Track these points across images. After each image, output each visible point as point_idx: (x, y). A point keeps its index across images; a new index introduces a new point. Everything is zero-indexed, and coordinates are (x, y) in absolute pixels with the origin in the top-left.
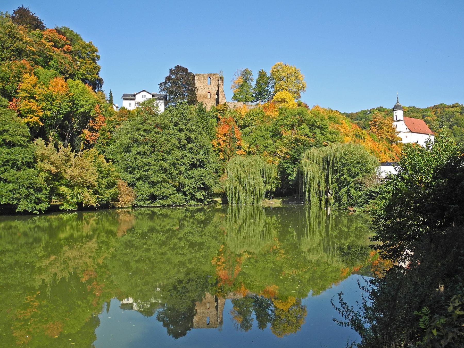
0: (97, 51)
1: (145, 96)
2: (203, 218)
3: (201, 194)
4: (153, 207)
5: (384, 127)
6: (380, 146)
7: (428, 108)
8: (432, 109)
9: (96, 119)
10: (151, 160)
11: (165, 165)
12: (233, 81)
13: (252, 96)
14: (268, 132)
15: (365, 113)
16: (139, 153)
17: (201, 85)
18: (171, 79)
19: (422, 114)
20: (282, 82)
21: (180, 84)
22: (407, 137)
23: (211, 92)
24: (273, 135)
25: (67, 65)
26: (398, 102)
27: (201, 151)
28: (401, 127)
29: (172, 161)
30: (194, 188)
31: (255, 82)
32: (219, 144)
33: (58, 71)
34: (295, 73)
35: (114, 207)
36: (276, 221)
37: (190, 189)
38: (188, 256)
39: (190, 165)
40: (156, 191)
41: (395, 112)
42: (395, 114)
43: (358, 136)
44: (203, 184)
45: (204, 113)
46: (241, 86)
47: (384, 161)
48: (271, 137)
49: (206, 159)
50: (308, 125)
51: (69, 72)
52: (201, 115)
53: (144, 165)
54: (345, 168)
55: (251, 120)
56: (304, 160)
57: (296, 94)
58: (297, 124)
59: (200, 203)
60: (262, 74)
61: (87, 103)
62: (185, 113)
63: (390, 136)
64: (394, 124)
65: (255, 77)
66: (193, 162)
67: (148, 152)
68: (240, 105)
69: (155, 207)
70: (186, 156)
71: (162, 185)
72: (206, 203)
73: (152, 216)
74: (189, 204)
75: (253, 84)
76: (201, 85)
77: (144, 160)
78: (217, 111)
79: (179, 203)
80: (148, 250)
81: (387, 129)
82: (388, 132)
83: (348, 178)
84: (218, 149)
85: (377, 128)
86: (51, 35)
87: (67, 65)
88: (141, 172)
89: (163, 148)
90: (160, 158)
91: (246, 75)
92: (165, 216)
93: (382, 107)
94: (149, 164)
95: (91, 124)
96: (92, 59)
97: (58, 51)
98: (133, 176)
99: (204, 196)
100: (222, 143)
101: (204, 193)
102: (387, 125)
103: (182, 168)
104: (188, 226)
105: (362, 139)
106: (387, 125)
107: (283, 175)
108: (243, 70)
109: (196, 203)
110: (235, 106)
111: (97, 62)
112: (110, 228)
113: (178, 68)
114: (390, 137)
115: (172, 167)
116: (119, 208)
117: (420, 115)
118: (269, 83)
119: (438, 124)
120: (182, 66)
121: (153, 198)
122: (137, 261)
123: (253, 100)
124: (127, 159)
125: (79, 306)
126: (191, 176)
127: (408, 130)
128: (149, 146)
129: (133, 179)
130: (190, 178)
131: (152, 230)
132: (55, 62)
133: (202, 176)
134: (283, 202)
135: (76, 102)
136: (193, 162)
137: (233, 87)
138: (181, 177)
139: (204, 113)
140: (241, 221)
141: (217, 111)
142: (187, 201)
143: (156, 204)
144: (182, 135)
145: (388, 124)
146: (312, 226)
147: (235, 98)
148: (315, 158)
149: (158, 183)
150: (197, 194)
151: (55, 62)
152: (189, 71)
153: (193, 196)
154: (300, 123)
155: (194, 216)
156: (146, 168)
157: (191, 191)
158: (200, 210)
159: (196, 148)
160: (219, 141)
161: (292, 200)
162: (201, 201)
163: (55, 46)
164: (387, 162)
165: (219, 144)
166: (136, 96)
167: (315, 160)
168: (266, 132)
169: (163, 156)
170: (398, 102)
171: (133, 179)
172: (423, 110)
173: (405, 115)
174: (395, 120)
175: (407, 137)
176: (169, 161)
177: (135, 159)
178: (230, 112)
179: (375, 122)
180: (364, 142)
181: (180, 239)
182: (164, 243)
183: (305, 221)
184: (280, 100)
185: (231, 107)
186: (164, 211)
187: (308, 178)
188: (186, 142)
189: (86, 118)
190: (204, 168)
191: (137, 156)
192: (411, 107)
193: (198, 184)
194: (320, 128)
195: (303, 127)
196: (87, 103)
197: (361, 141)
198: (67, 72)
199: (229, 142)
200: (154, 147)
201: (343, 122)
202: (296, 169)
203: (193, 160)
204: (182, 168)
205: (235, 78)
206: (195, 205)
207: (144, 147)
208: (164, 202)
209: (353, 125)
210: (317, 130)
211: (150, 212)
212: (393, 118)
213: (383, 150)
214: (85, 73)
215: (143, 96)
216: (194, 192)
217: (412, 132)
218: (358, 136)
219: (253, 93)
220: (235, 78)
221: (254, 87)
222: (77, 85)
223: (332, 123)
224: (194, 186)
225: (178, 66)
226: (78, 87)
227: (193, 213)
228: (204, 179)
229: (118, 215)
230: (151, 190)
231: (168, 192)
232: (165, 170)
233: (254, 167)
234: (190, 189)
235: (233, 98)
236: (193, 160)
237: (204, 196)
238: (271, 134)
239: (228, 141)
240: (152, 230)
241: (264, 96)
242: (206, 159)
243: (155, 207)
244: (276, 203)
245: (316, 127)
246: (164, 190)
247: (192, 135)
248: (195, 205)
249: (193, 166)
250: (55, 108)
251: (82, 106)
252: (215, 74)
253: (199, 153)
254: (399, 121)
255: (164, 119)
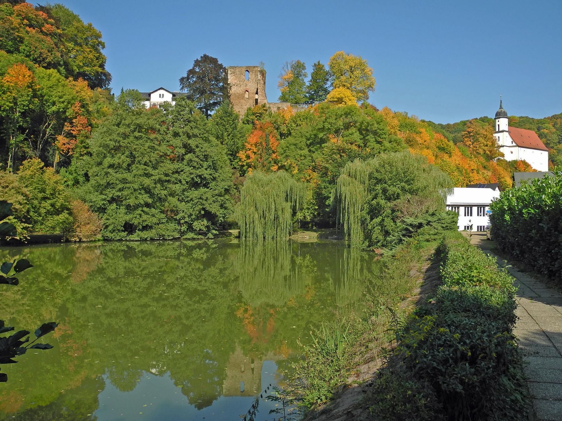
0: (100, 37)
1: (163, 95)
2: (205, 257)
3: (202, 223)
4: (130, 241)
5: (480, 139)
6: (472, 163)
7: (545, 118)
8: (551, 120)
9: (74, 121)
10: (128, 176)
11: (147, 182)
12: (281, 76)
13: (306, 96)
14: (304, 140)
15: (464, 123)
16: (111, 166)
17: (236, 81)
18: (196, 72)
19: (538, 126)
20: (343, 78)
21: (207, 81)
22: (512, 153)
23: (249, 91)
24: (311, 144)
25: (45, 51)
26: (501, 108)
27: (205, 164)
28: (504, 139)
29: (157, 178)
30: (191, 215)
31: (310, 78)
32: (248, 157)
33: (31, 57)
34: (361, 66)
35: (68, 241)
36: (311, 262)
37: (186, 216)
38: (185, 310)
39: (187, 183)
40: (135, 218)
41: (497, 120)
42: (497, 123)
43: (442, 149)
44: (204, 209)
45: (229, 116)
46: (291, 84)
47: (476, 182)
48: (308, 146)
49: (210, 175)
50: (360, 130)
51: (47, 60)
52: (225, 119)
53: (118, 182)
54: (379, 187)
55: (297, 126)
56: (343, 177)
57: (363, 94)
58: (343, 127)
59: (200, 236)
60: (318, 67)
61: (61, 100)
62: (182, 111)
63: (489, 151)
64: (496, 135)
65: (309, 70)
66: (193, 179)
67: (125, 165)
68: (286, 106)
69: (133, 241)
70: (182, 171)
71: (142, 211)
72: (210, 235)
73: (129, 253)
74: (185, 237)
75: (307, 80)
76: (236, 81)
77: (119, 176)
78: (254, 114)
79: (169, 236)
80: (123, 301)
81: (485, 142)
82: (487, 146)
83: (383, 202)
84: (247, 164)
85: (472, 141)
86: (24, 10)
87: (45, 51)
88: (114, 191)
89: (145, 159)
90: (141, 172)
91: (298, 68)
92: (146, 253)
93: (487, 117)
94: (124, 181)
95: (67, 127)
96: (93, 47)
97: (33, 31)
98: (104, 197)
99: (207, 227)
100: (252, 155)
101: (205, 222)
102: (485, 137)
103: (177, 188)
104: (182, 268)
105: (447, 153)
106: (485, 137)
107: (320, 198)
108: (294, 63)
109: (195, 237)
110: (279, 108)
111: (102, 51)
112: (55, 270)
113: (205, 58)
114: (488, 153)
115: (158, 185)
116: (75, 242)
117: (535, 127)
118: (327, 80)
119: (557, 138)
120: (210, 56)
121: (129, 228)
122: (109, 315)
123: (308, 102)
124: (95, 174)
125: (48, 371)
126: (189, 199)
127: (514, 144)
128: (127, 157)
129: (102, 202)
130: (188, 201)
131: (129, 273)
132: (26, 46)
133: (201, 198)
134: (320, 237)
135: (46, 97)
136: (193, 179)
137: (281, 85)
138: (173, 201)
139: (229, 116)
140: (256, 262)
141: (254, 114)
142: (183, 233)
143: (134, 237)
144: (177, 142)
145: (487, 135)
146: (351, 272)
147: (284, 99)
148: (358, 174)
149: (136, 207)
150: (195, 223)
151: (26, 46)
152: (219, 63)
153: (190, 228)
154: (347, 127)
155: (191, 255)
156: (120, 186)
157: (187, 219)
158: (199, 247)
159: (197, 159)
160: (249, 152)
161: (332, 234)
162: (200, 233)
163: (31, 26)
164: (480, 184)
165: (248, 157)
166: (152, 95)
167: (358, 177)
168: (300, 139)
169: (145, 170)
170: (501, 108)
171: (102, 202)
172: (538, 120)
173: (510, 125)
174: (497, 130)
175: (512, 153)
176: (153, 178)
177: (107, 173)
178: (270, 115)
179: (469, 133)
180: (450, 157)
181: (170, 286)
182: (146, 292)
183: (343, 266)
184: (336, 100)
185: (274, 110)
186: (145, 247)
187: (347, 203)
188: (183, 151)
189: (61, 118)
190: (208, 188)
191: (110, 170)
192: (523, 117)
193: (195, 209)
194: (375, 133)
195: (350, 131)
196: (61, 100)
197: (446, 157)
198: (44, 59)
199: (260, 154)
200: (132, 156)
201: (423, 130)
202: (333, 191)
203: (192, 176)
204: (177, 188)
205: (283, 73)
206: (193, 239)
207: (120, 158)
208: (145, 234)
209: (436, 135)
210: (371, 137)
211: (125, 248)
212: (495, 129)
213: (475, 168)
214: (81, 64)
215: (160, 95)
216: (192, 220)
217: (519, 147)
218: (442, 149)
219: (307, 93)
220: (283, 73)
221: (308, 84)
222: (50, 75)
223: (408, 132)
224: (191, 212)
225: (205, 55)
226: (51, 78)
227: (190, 250)
228: (204, 202)
229: (73, 252)
230: (128, 218)
231: (151, 220)
232: (148, 191)
233: (276, 187)
234: (186, 216)
235: (280, 99)
236: (192, 176)
237: (207, 227)
238: (308, 142)
239: (259, 152)
240: (129, 273)
241: (321, 96)
242: (210, 175)
243: (133, 241)
244: (310, 237)
245: (370, 132)
246: (145, 217)
247: (192, 143)
248: (193, 239)
249: (195, 185)
250: (7, 103)
251: (54, 104)
252: (254, 67)
253: (202, 167)
254: (503, 131)
255: (148, 119)
